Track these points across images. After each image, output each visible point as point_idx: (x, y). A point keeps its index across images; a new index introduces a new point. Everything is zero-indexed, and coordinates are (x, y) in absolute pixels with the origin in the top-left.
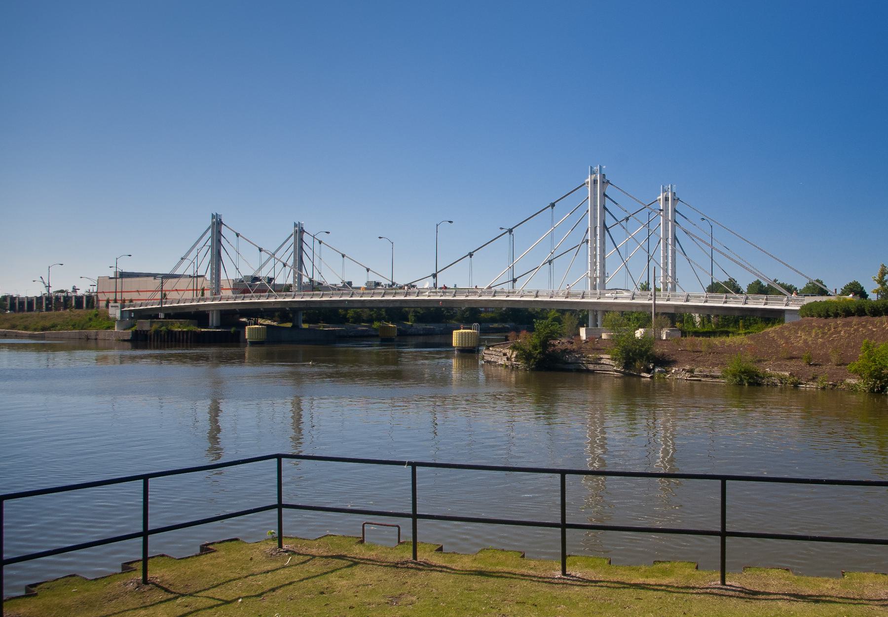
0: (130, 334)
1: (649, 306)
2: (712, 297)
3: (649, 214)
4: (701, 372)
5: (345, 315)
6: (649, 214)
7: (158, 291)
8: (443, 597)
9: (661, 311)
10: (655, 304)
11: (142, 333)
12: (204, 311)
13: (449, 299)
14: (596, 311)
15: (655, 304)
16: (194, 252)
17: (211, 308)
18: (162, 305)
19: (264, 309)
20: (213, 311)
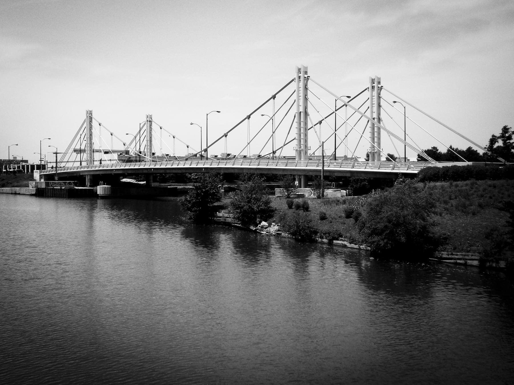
0: (35, 190)
1: (319, 171)
2: (311, 163)
3: (336, 101)
4: (130, 266)
5: (190, 177)
6: (336, 101)
7: (58, 162)
8: (279, 297)
9: (328, 174)
10: (323, 170)
11: (41, 189)
12: (83, 176)
13: (317, 169)
14: (294, 176)
15: (323, 170)
16: (79, 136)
17: (86, 174)
18: (56, 172)
19: (127, 173)
20: (88, 175)
